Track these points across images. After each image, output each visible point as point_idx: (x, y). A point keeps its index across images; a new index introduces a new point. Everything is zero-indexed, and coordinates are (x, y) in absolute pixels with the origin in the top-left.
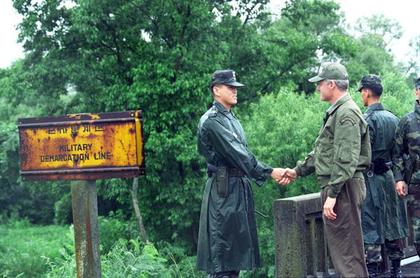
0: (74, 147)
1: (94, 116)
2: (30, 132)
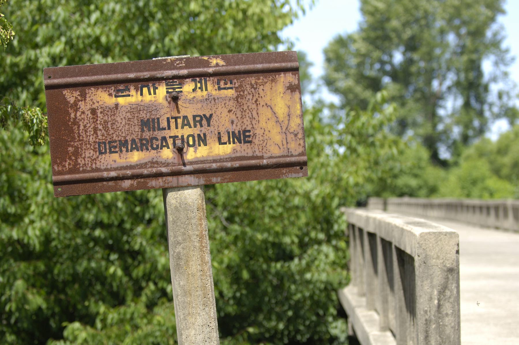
0: (172, 122)
1: (214, 61)
2: (71, 96)
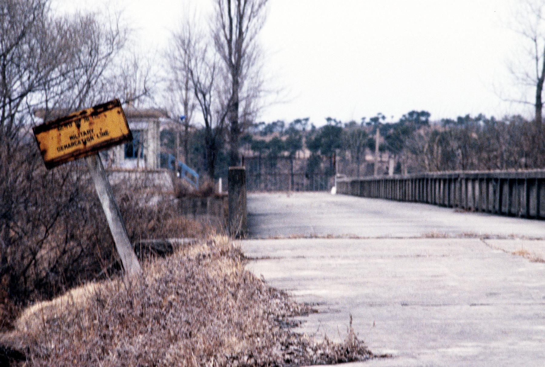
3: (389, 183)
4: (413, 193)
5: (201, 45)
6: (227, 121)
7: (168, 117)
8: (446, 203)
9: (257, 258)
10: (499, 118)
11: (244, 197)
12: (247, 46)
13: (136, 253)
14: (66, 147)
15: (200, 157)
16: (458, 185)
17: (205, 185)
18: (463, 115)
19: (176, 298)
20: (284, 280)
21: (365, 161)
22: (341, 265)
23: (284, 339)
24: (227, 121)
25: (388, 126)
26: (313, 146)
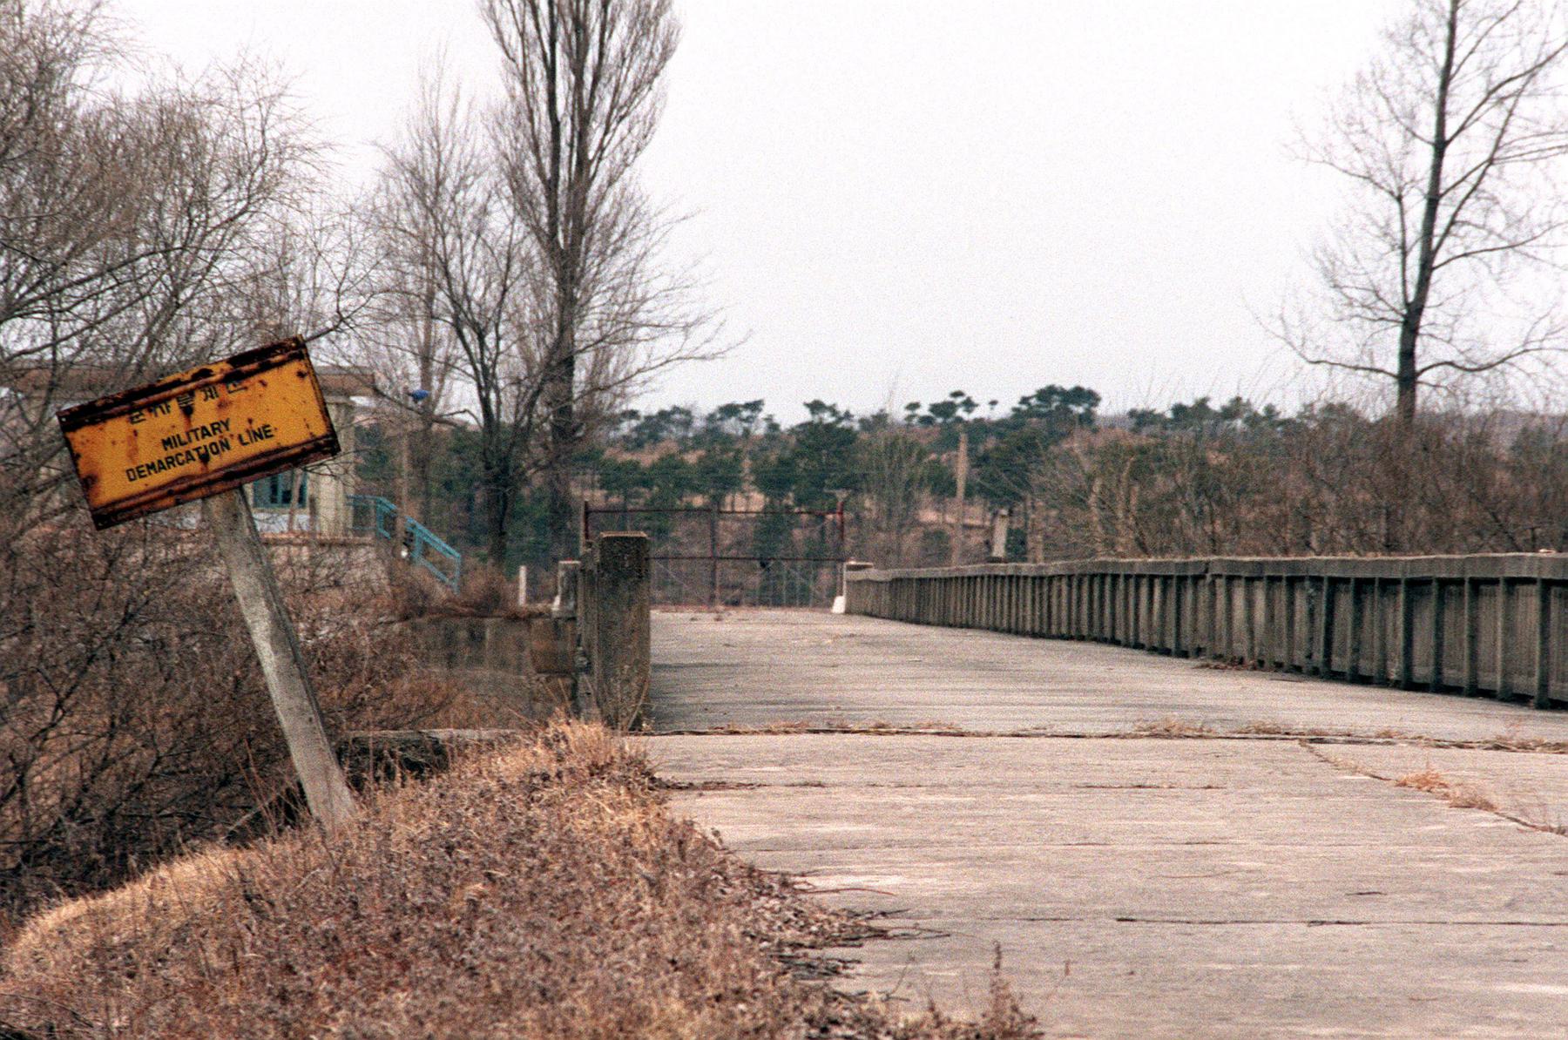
0: (192, 435)
3: (1002, 586)
4: (1074, 616)
5: (476, 193)
6: (541, 409)
7: (377, 393)
8: (1171, 644)
9: (691, 786)
10: (1289, 408)
11: (644, 617)
12: (602, 198)
13: (340, 764)
14: (151, 467)
15: (455, 505)
16: (1204, 594)
17: (477, 584)
18: (1189, 402)
19: (487, 890)
20: (777, 845)
21: (917, 523)
22: (926, 807)
23: (814, 1007)
24: (541, 409)
25: (981, 428)
26: (772, 482)
